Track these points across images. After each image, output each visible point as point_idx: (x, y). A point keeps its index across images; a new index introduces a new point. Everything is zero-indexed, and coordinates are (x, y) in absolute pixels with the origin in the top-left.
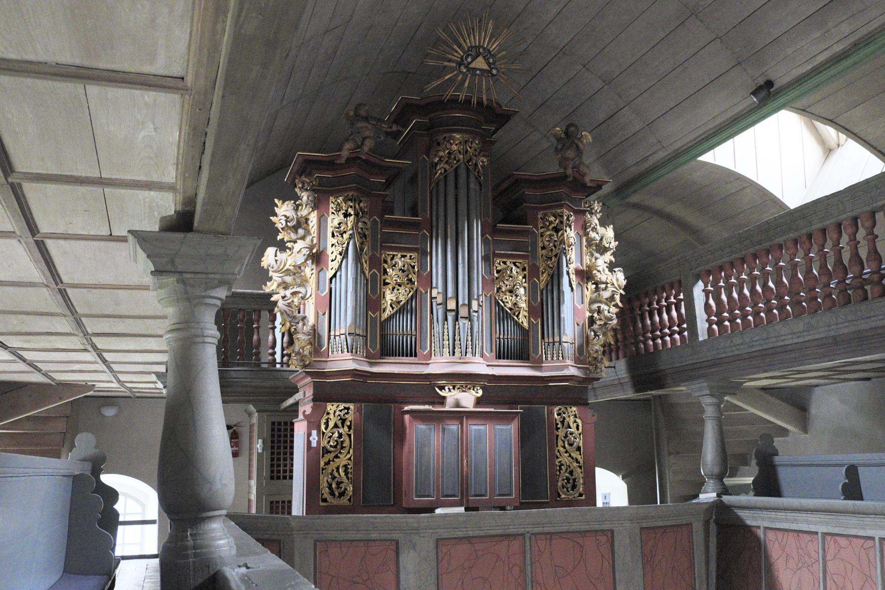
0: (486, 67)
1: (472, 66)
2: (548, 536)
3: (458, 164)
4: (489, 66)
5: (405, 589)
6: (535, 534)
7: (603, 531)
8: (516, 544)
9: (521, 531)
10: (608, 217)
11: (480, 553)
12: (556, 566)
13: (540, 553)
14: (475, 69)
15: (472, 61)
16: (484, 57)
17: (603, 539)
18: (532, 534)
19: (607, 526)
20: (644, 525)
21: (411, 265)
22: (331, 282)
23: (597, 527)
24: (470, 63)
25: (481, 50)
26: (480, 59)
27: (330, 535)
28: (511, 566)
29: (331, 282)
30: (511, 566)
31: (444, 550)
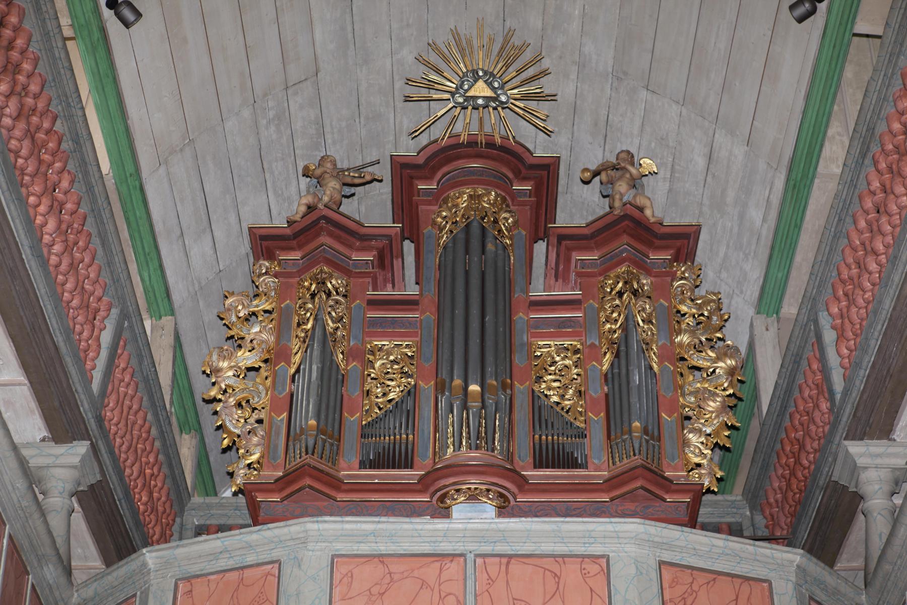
0: (489, 93)
1: (469, 94)
2: (504, 560)
3: (469, 220)
4: (495, 93)
5: (31, 2)
6: (484, 556)
7: (594, 558)
8: (453, 568)
9: (459, 548)
10: (767, 330)
11: (396, 577)
12: (514, 599)
13: (490, 581)
14: (475, 98)
15: (470, 88)
16: (485, 82)
17: (593, 568)
18: (477, 556)
19: (597, 549)
20: (667, 557)
21: (407, 355)
22: (293, 380)
23: (580, 549)
24: (466, 91)
25: (481, 73)
26: (481, 84)
27: (195, 569)
28: (443, 595)
29: (293, 380)
30: (443, 595)
31: (344, 571)
